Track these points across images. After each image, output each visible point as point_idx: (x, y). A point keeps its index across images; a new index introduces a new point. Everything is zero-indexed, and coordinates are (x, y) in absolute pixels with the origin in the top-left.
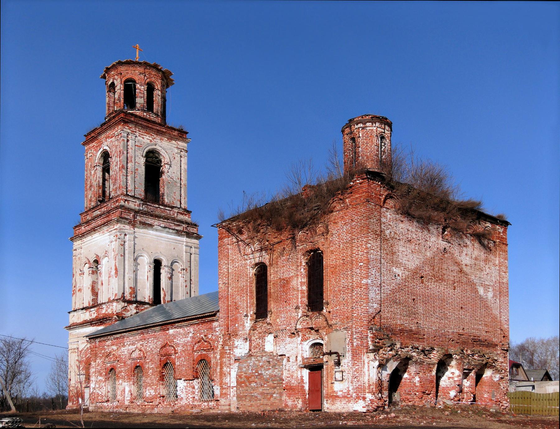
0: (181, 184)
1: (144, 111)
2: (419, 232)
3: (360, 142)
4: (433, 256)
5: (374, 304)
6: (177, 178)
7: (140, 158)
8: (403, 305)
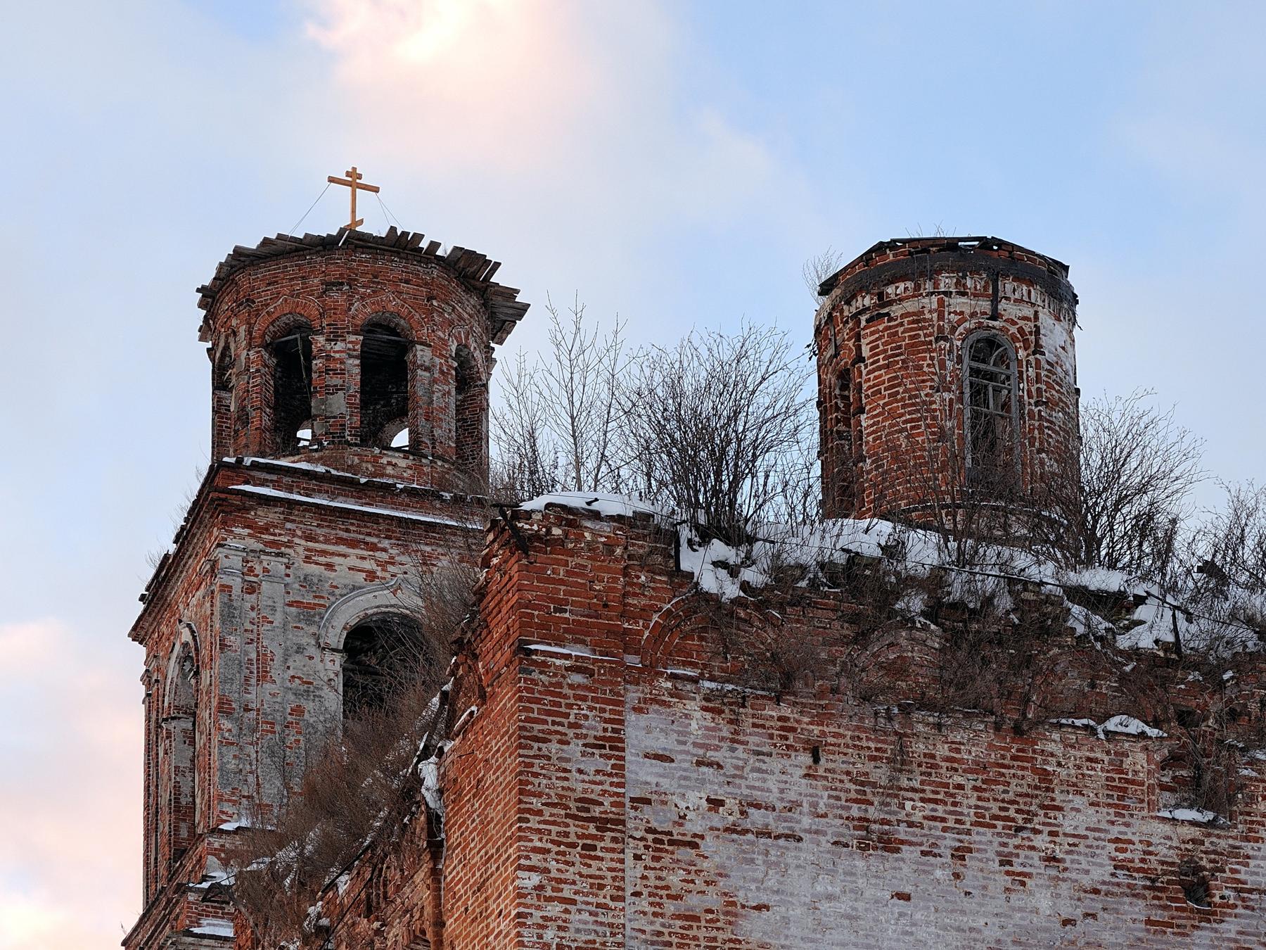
2: (960, 787)
3: (865, 386)
7: (311, 658)
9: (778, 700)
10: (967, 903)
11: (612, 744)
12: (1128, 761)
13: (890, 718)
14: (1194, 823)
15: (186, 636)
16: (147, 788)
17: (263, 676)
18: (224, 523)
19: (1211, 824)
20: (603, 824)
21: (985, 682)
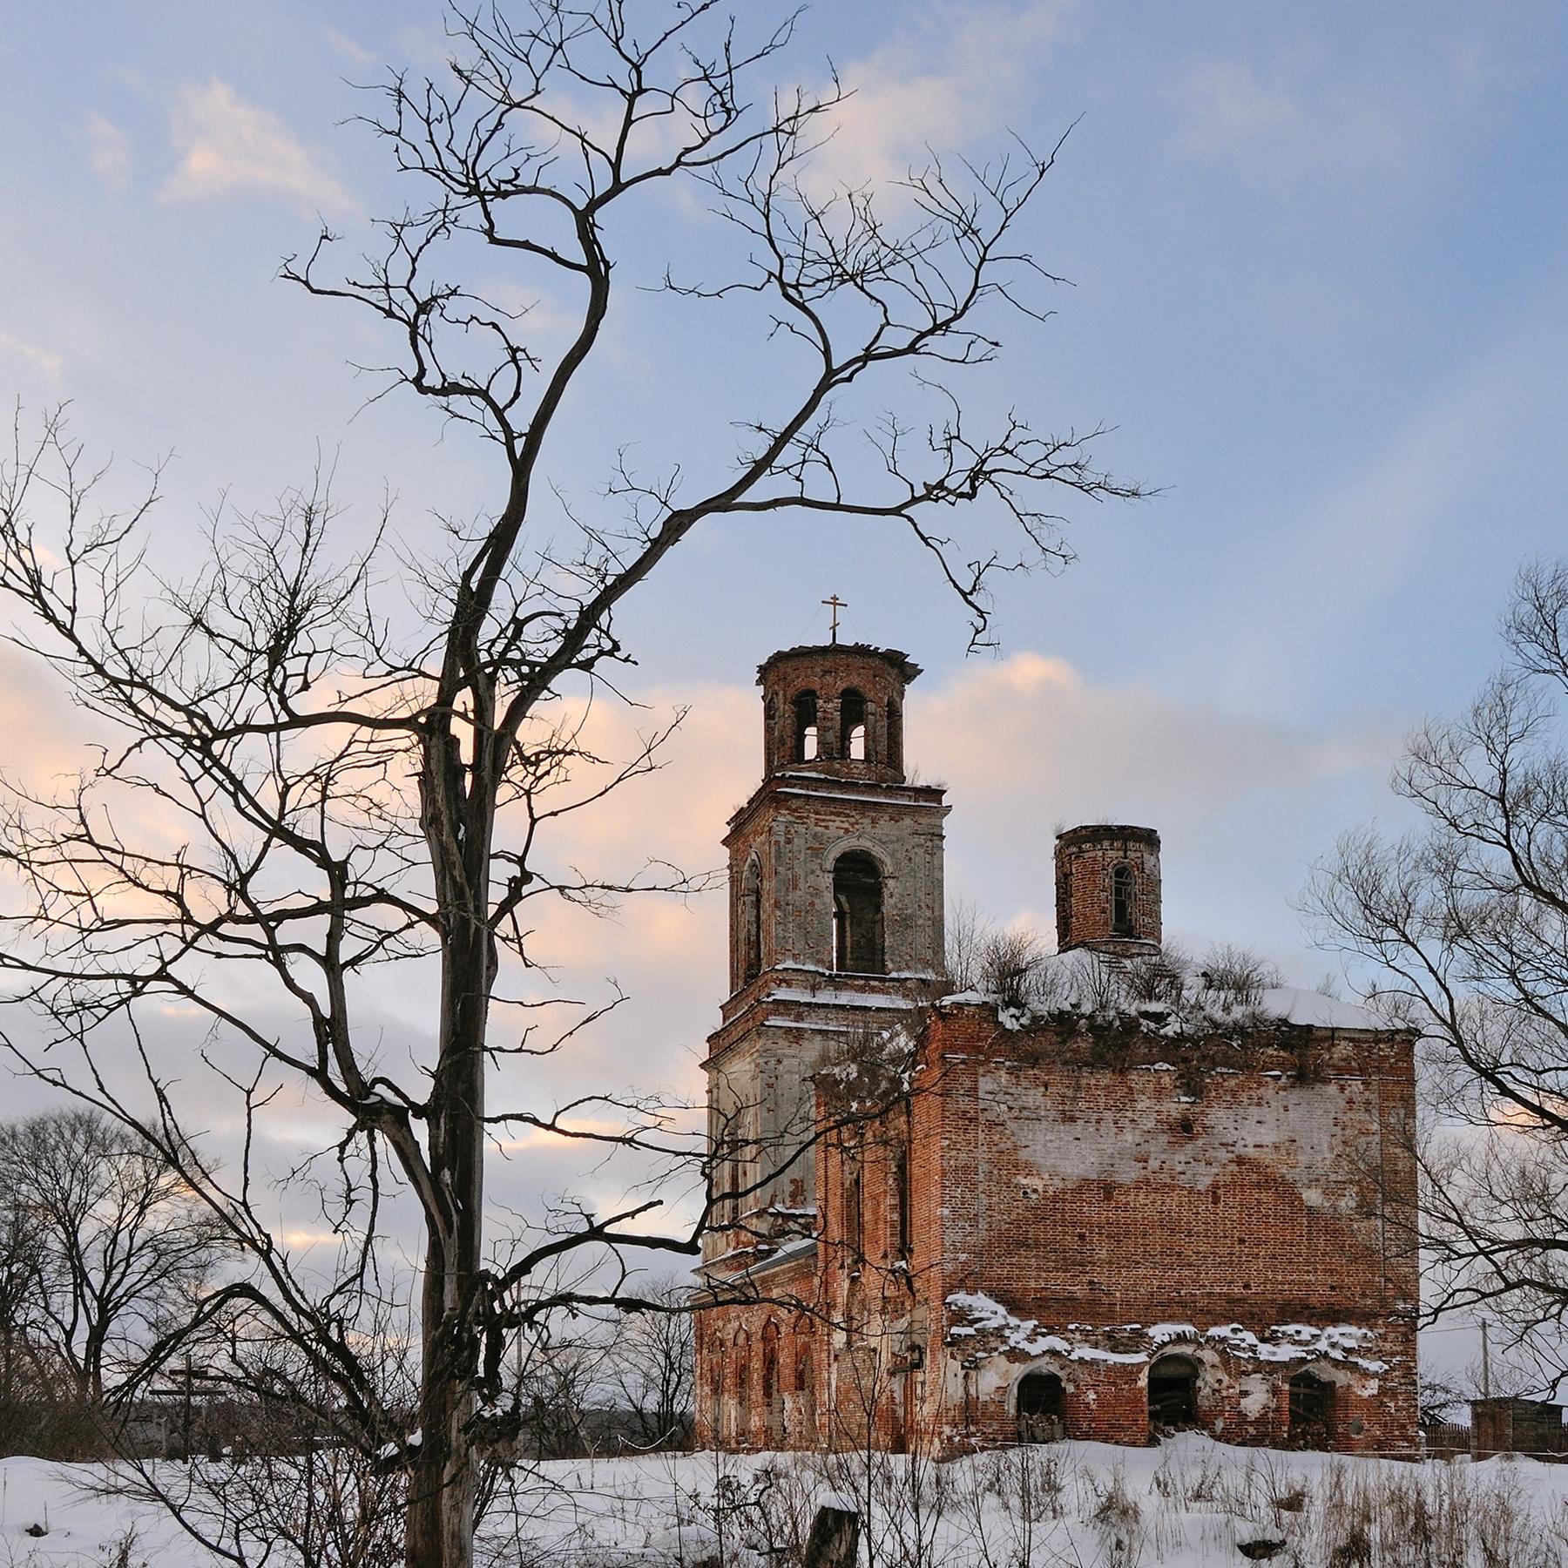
9: (1033, 1068)
10: (1102, 1140)
11: (973, 1092)
12: (1162, 1081)
13: (1073, 1072)
14: (1187, 1103)
15: (754, 856)
16: (731, 926)
17: (795, 888)
18: (776, 807)
19: (1194, 1102)
20: (970, 1120)
21: (1110, 1056)
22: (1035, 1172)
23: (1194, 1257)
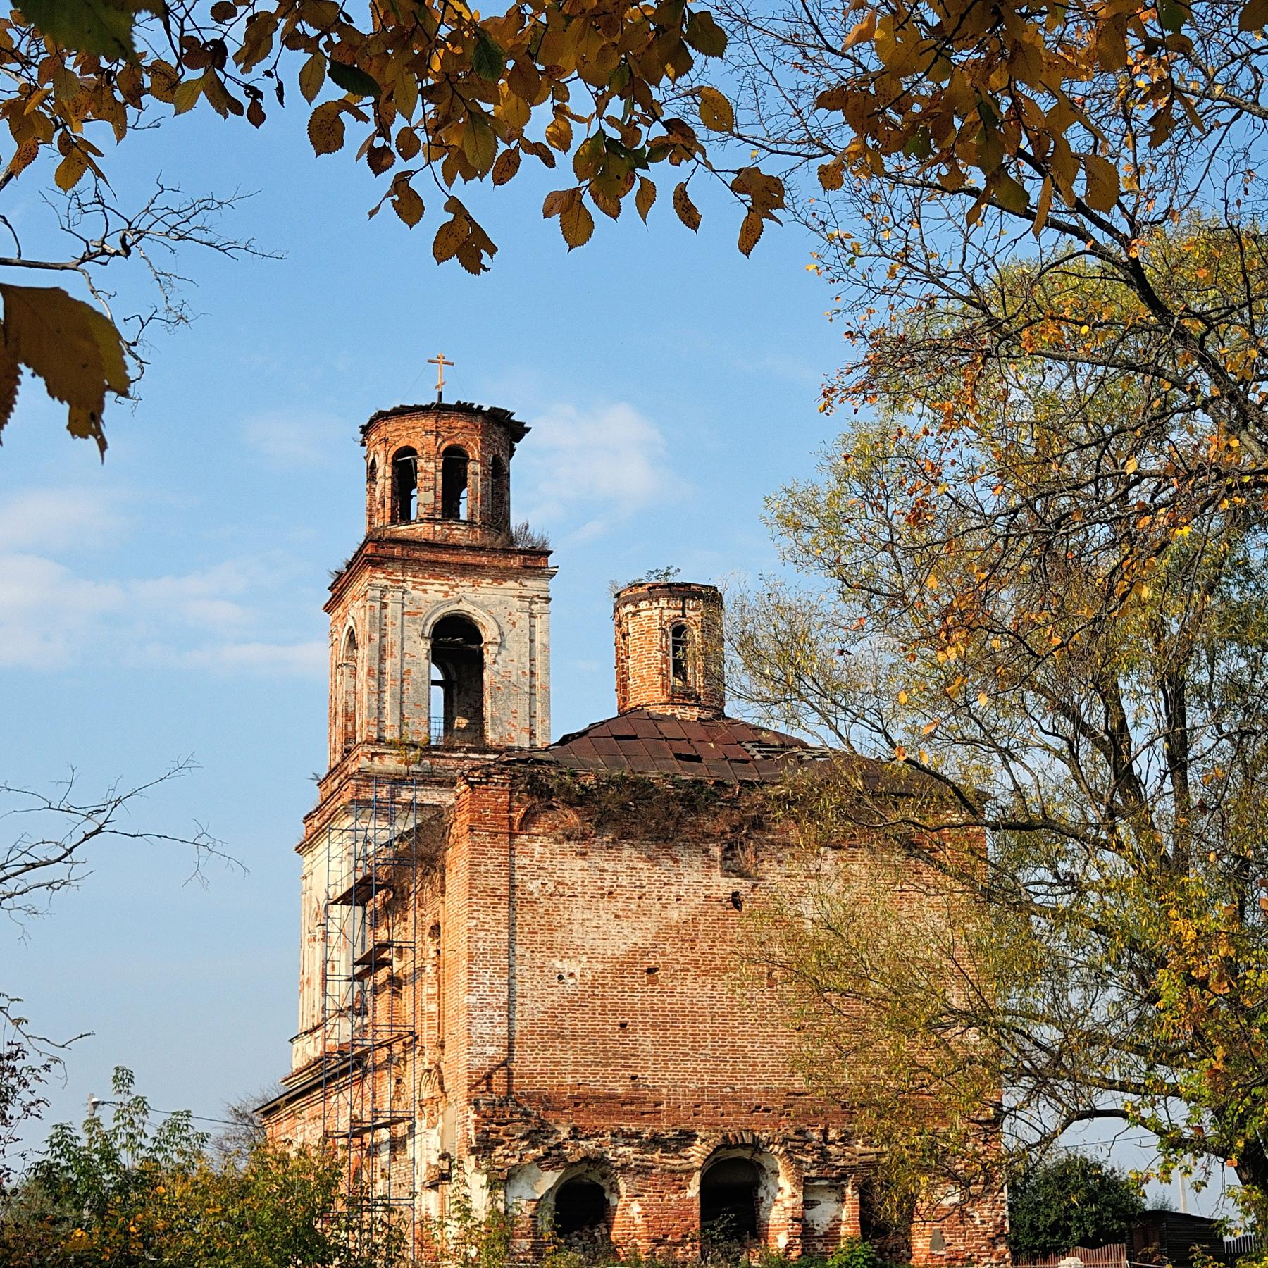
0: (532, 686)
1: (435, 521)
2: (642, 869)
4: (690, 918)
5: (487, 1048)
6: (520, 672)
8: (586, 1041)
15: (351, 623)
22: (571, 954)
23: (749, 1048)
